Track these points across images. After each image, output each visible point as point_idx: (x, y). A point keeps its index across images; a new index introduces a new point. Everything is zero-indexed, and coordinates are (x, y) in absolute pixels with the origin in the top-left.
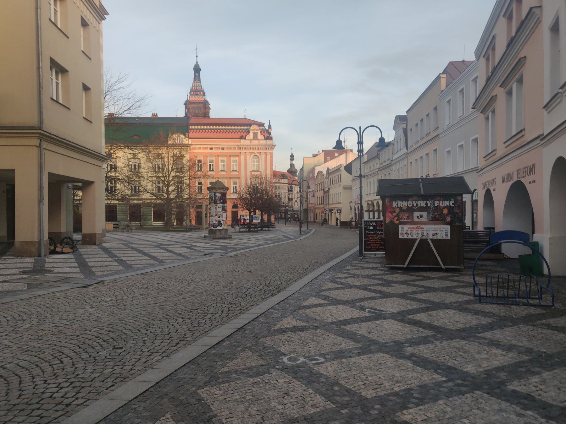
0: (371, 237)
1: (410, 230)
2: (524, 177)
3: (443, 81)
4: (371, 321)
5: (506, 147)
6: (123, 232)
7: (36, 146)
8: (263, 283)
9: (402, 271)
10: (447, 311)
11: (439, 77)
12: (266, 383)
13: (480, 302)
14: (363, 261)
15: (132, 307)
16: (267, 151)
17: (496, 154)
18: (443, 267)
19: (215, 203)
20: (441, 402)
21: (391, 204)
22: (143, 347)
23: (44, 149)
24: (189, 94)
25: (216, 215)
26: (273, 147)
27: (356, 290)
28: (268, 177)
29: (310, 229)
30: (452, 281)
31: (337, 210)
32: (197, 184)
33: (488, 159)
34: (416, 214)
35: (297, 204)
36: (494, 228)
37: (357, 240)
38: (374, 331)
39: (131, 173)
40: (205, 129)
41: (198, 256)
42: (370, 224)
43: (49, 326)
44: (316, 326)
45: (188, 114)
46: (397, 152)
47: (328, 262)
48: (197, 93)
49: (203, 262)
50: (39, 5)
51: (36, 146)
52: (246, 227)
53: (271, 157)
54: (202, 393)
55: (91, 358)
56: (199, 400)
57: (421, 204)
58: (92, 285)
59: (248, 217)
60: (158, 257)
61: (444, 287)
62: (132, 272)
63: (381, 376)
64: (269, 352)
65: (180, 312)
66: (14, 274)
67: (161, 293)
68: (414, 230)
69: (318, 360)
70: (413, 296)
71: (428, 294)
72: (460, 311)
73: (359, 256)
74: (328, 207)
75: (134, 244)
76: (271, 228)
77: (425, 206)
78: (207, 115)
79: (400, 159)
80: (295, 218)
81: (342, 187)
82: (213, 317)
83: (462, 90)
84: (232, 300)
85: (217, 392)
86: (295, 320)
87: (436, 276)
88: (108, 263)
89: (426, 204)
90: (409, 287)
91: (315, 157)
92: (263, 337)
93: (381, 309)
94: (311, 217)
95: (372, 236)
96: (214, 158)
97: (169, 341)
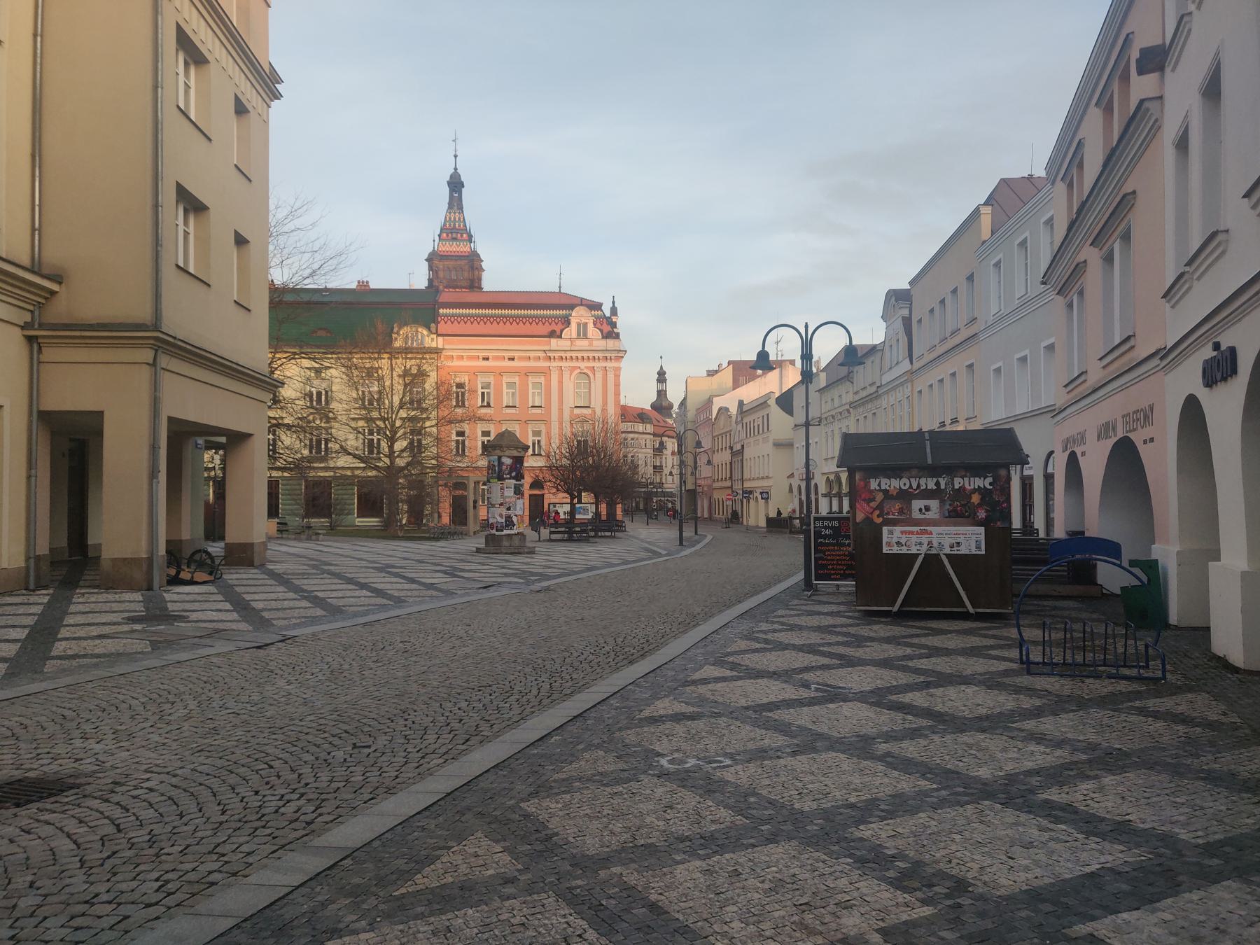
0: (829, 550)
1: (904, 536)
2: (1135, 430)
3: (986, 221)
4: (820, 704)
5: (1104, 367)
6: (300, 540)
7: (148, 364)
8: (611, 641)
9: (889, 619)
10: (963, 687)
11: (976, 213)
12: (633, 793)
13: (1029, 673)
14: (813, 600)
15: (365, 683)
16: (609, 364)
17: (1085, 381)
18: (971, 610)
19: (501, 478)
20: (922, 815)
21: (866, 485)
22: (406, 746)
23: (163, 369)
24: (437, 239)
25: (501, 504)
26: (620, 354)
27: (794, 653)
28: (609, 421)
29: (700, 535)
30: (985, 636)
31: (761, 493)
32: (454, 437)
33: (1072, 390)
34: (917, 504)
35: (673, 480)
36: (1083, 533)
37: (801, 559)
38: (823, 720)
39: (312, 411)
40: (472, 316)
41: (470, 589)
42: (826, 523)
43: (221, 713)
44: (716, 713)
45: (436, 283)
46: (891, 368)
47: (740, 602)
48: (454, 235)
49: (484, 602)
50: (160, 79)
51: (148, 364)
52: (563, 529)
53: (617, 376)
54: (530, 807)
55: (320, 761)
56: (526, 816)
57: (926, 485)
58: (272, 644)
59: (567, 508)
60: (389, 592)
61: (967, 648)
62: (344, 619)
63: (829, 783)
64: (635, 752)
65: (459, 691)
66: (114, 624)
67: (414, 659)
68: (914, 536)
69: (721, 762)
70: (904, 663)
71: (934, 660)
72: (989, 688)
73: (804, 591)
74: (740, 486)
75: (331, 565)
76: (618, 531)
77: (935, 488)
78: (477, 285)
79: (896, 385)
80: (668, 510)
81: (771, 443)
82: (525, 699)
83: (1025, 241)
84: (553, 670)
85: (553, 806)
86: (677, 704)
87: (956, 628)
88: (292, 604)
89: (938, 484)
90: (900, 647)
91: (713, 375)
92: (620, 730)
93: (841, 685)
94: (703, 508)
95: (830, 548)
96: (491, 379)
97: (451, 736)
